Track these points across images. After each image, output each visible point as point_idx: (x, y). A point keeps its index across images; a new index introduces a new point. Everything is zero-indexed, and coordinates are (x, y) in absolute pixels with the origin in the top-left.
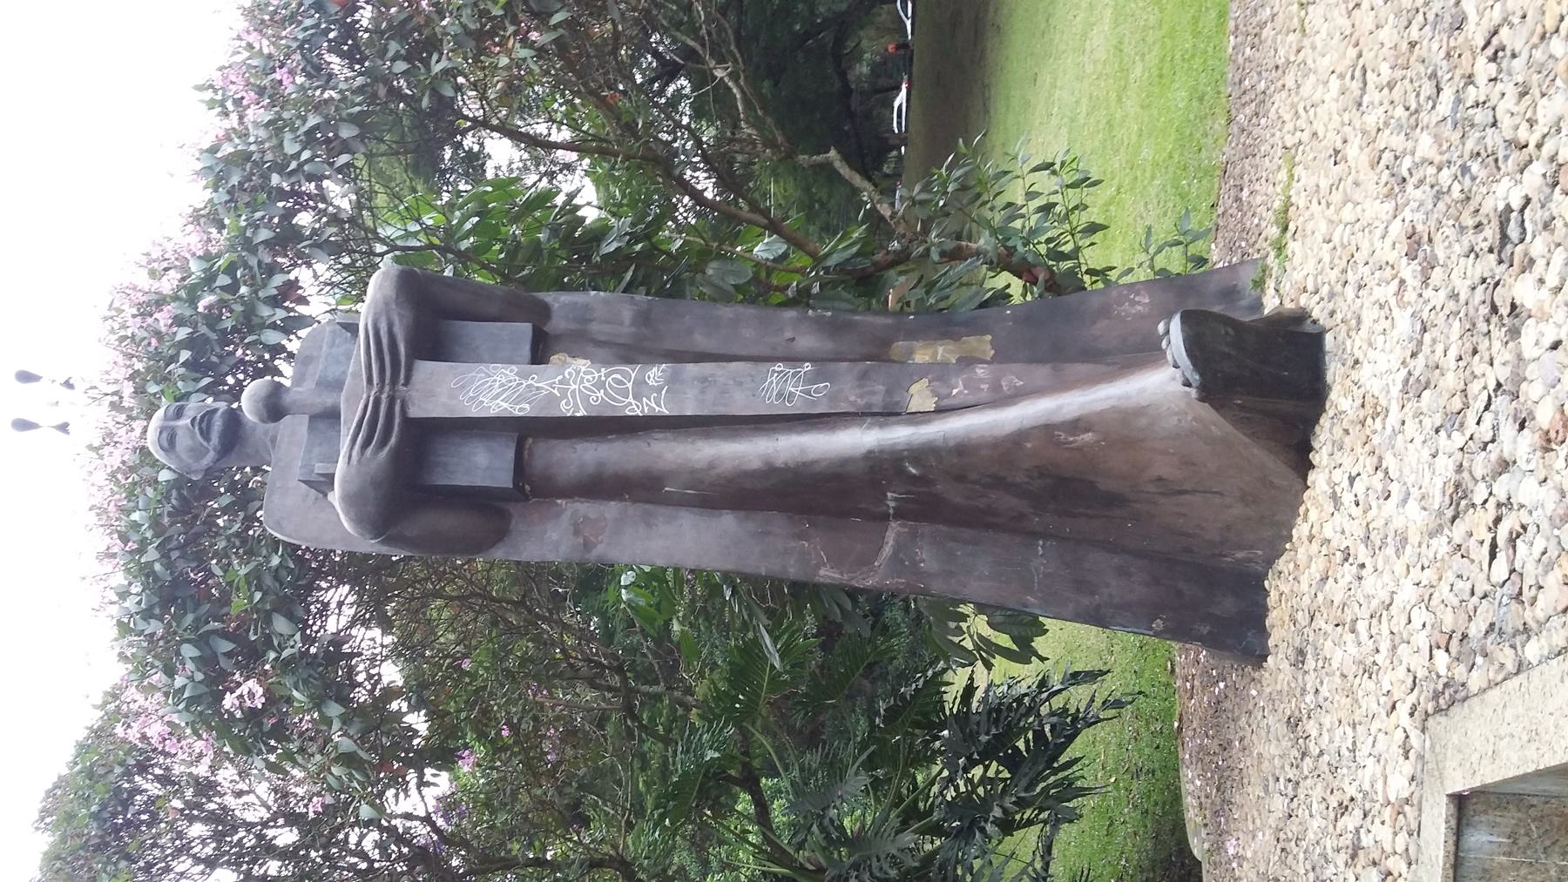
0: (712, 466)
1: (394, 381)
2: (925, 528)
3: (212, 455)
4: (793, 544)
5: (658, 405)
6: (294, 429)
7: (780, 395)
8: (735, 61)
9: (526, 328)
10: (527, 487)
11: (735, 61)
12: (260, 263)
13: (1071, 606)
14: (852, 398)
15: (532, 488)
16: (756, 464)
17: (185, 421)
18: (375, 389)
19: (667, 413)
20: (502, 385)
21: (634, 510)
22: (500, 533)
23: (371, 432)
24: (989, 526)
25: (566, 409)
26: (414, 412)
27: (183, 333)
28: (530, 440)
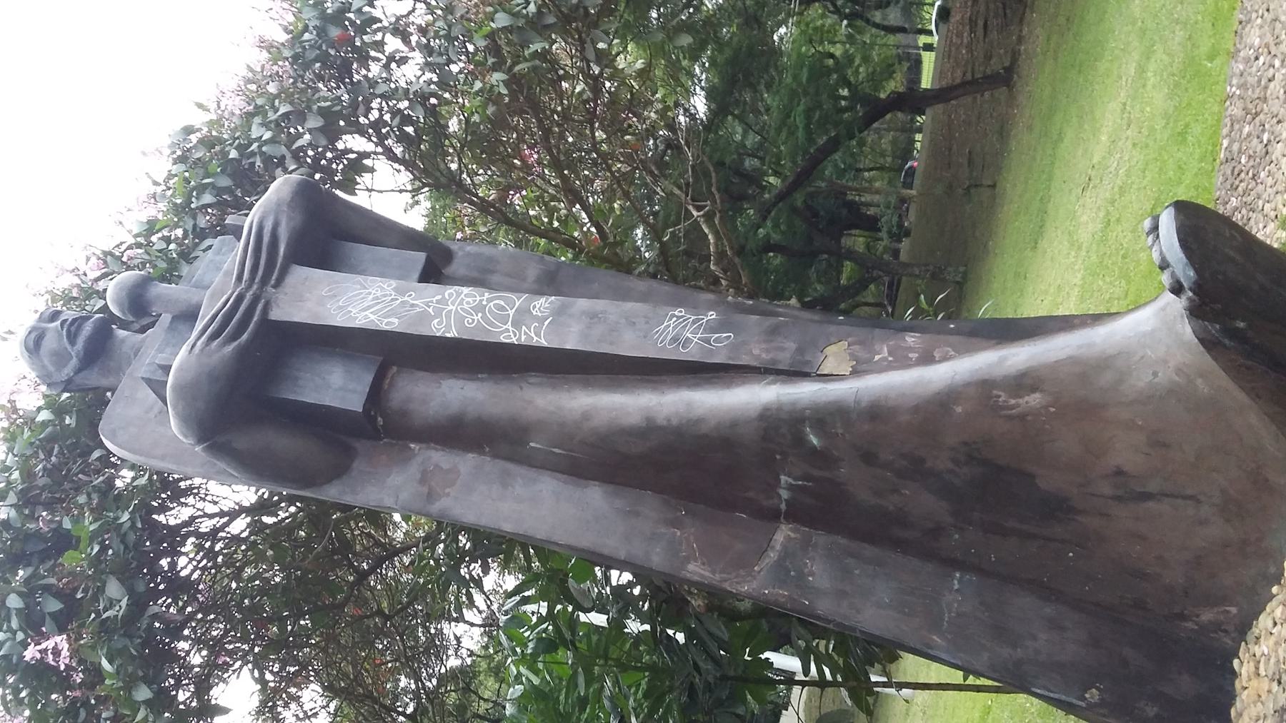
0: (586, 416)
1: (265, 281)
2: (820, 538)
3: (74, 362)
5: (538, 335)
7: (675, 339)
8: (714, 202)
9: (421, 256)
11: (714, 202)
12: (195, 226)
13: (986, 655)
14: (756, 352)
16: (634, 419)
19: (544, 343)
20: (377, 298)
21: (491, 466)
22: (338, 471)
23: (223, 327)
24: (899, 545)
26: (276, 314)
28: (395, 369)
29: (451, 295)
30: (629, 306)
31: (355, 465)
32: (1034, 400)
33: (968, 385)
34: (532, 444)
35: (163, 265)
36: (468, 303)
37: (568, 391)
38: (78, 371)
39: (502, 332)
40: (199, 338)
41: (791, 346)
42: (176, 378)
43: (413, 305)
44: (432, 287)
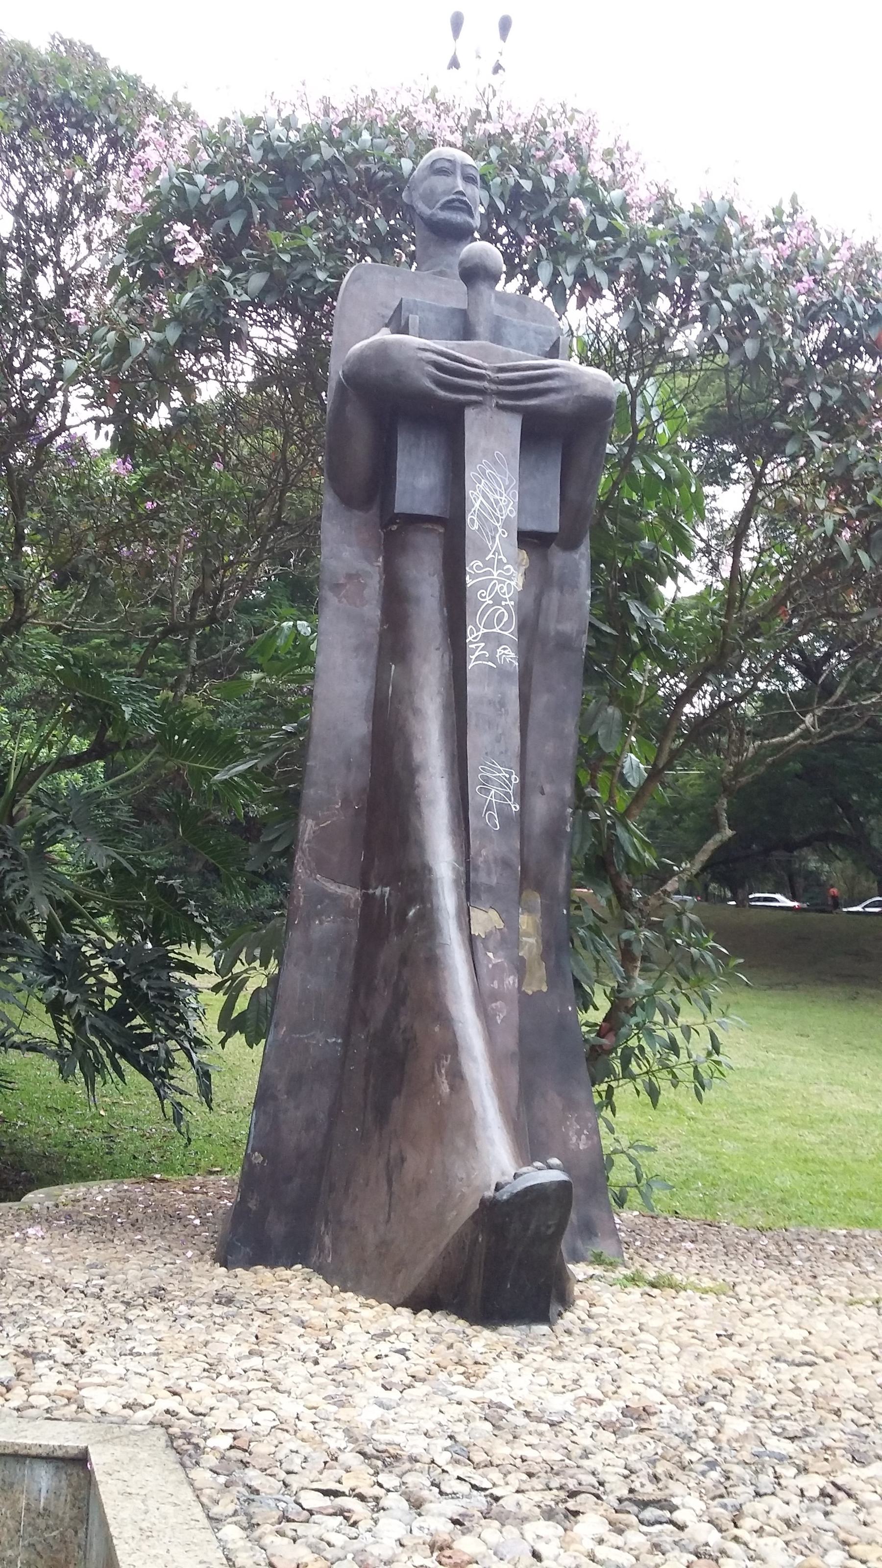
0: (416, 711)
2: (354, 925)
3: (427, 212)
5: (477, 659)
6: (452, 294)
7: (487, 780)
8: (821, 735)
9: (553, 525)
10: (395, 527)
15: (394, 532)
16: (418, 756)
17: (461, 185)
20: (497, 502)
21: (372, 633)
22: (348, 500)
23: (451, 372)
25: (473, 566)
26: (470, 414)
27: (549, 183)
28: (442, 530)
29: (508, 570)
31: (356, 512)
32: (445, 1088)
33: (454, 1034)
37: (439, 692)
39: (476, 626)
40: (433, 352)
41: (494, 880)
43: (494, 538)
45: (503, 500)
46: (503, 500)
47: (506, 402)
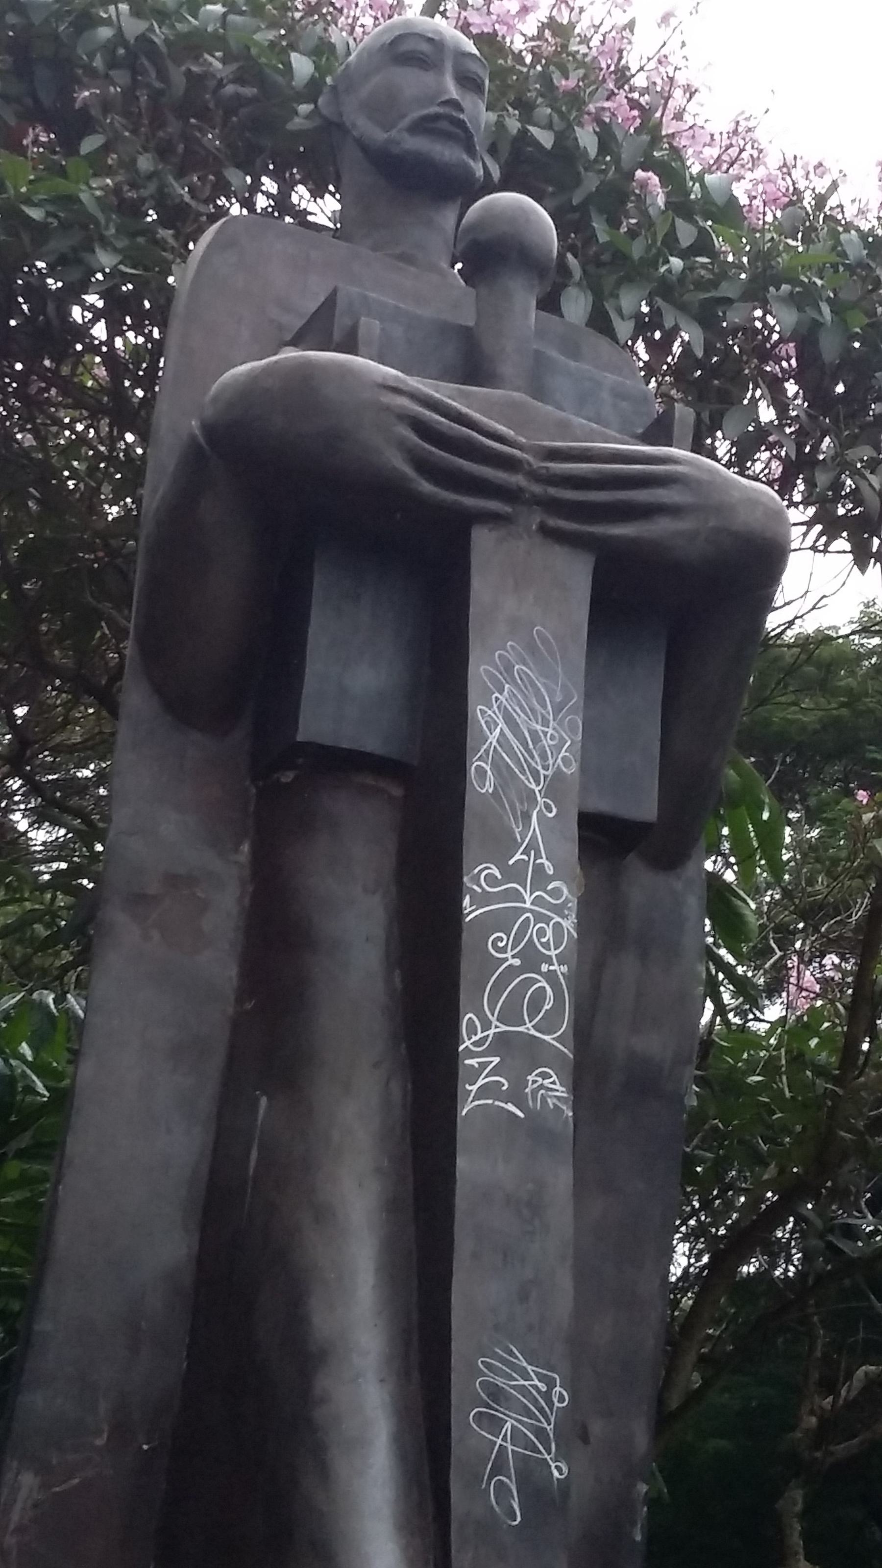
0: (324, 1214)
1: (553, 506)
3: (378, 135)
4: (103, 1407)
5: (483, 1092)
6: (446, 293)
7: (496, 1394)
9: (646, 807)
10: (288, 777)
15: (278, 782)
16: (322, 1322)
17: (453, 91)
18: (536, 464)
20: (536, 739)
22: (181, 706)
23: (446, 444)
25: (481, 876)
26: (482, 539)
27: (587, 139)
28: (397, 792)
29: (556, 893)
30: (565, 1282)
34: (264, 1101)
35: (637, 250)
36: (541, 933)
38: (364, 147)
42: (325, 367)
43: (527, 817)
44: (570, 849)
45: (549, 734)
46: (549, 734)
47: (554, 522)
